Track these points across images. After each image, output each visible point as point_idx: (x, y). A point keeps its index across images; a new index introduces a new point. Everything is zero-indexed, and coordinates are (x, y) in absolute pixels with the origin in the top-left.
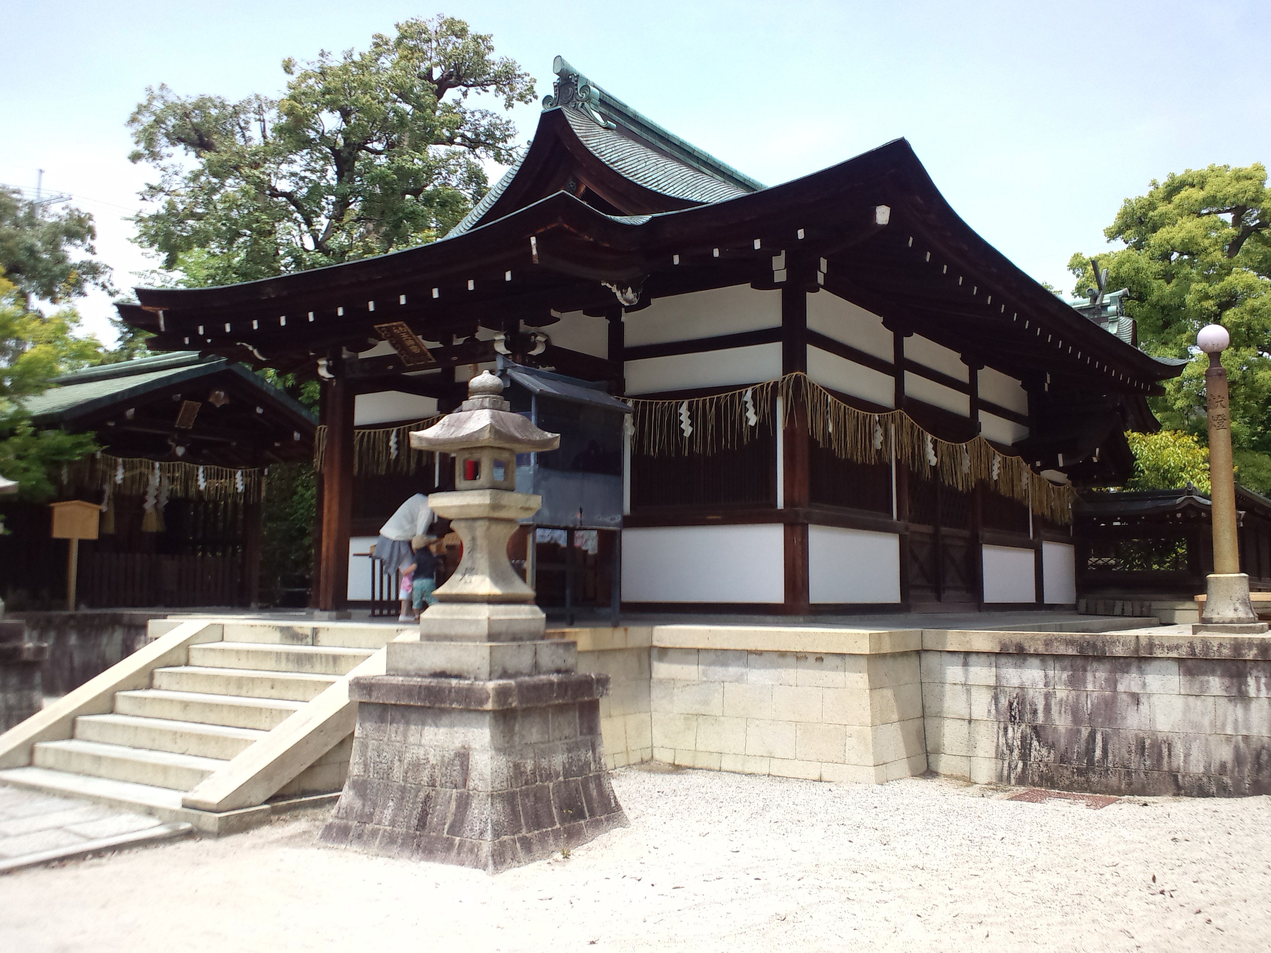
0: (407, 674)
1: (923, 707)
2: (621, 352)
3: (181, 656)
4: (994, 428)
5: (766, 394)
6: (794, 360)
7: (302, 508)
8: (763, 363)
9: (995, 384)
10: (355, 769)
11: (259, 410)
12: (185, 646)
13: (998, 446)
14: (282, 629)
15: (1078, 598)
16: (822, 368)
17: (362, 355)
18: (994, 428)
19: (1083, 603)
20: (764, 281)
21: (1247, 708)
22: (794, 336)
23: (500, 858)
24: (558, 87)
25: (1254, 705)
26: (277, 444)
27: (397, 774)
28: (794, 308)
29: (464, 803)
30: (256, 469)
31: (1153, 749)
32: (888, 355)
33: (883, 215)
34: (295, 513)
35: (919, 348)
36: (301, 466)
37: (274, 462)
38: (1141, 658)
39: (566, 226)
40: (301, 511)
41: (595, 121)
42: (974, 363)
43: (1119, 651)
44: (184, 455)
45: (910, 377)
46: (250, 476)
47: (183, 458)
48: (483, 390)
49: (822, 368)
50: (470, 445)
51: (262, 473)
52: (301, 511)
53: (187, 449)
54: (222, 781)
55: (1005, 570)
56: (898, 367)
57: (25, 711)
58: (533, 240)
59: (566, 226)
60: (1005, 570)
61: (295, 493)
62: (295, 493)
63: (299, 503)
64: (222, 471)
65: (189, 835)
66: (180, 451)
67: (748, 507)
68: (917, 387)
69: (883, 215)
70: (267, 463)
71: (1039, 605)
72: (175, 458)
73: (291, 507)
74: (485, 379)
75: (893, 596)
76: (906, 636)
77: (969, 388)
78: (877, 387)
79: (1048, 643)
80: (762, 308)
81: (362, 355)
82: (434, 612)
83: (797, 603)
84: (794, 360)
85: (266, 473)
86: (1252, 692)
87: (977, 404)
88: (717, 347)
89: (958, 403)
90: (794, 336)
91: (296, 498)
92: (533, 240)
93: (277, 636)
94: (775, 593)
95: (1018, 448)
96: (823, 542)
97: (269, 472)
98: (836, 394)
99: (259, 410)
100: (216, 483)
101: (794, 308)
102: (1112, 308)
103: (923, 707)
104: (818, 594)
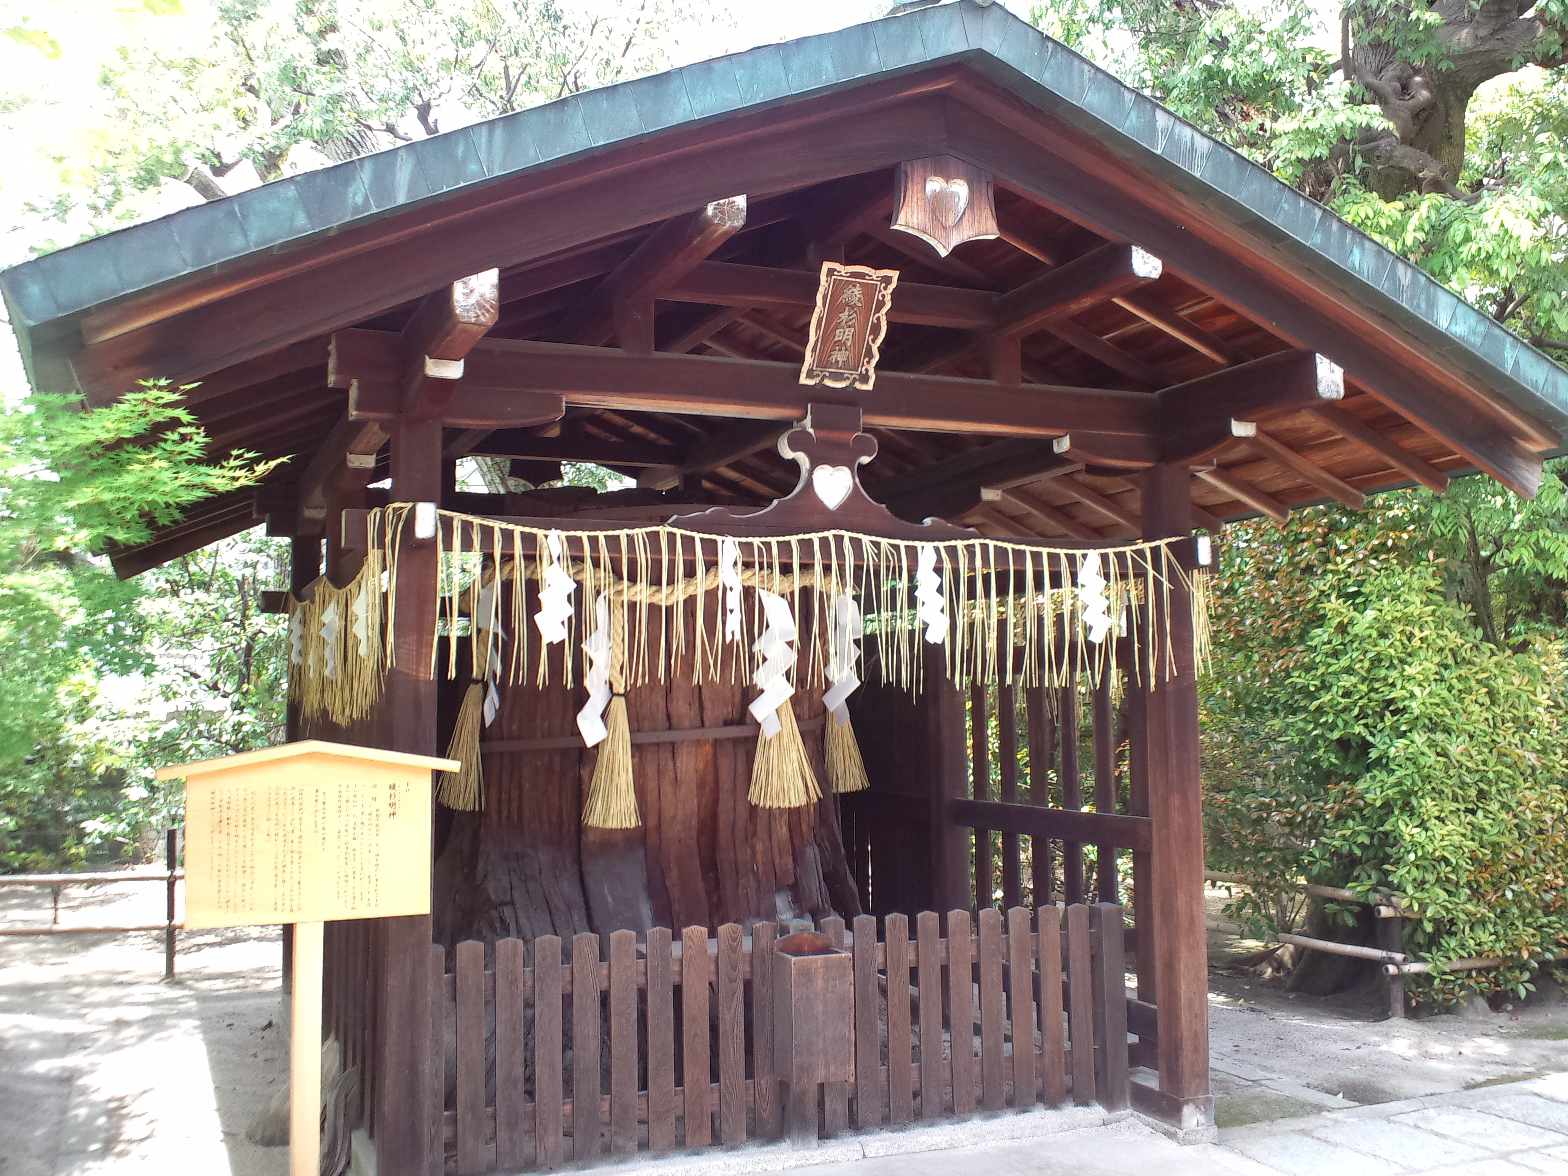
1: (660, 819)
7: (1349, 670)
11: (1146, 265)
26: (1241, 429)
30: (1162, 543)
34: (1325, 686)
36: (1334, 527)
37: (1236, 512)
39: (323, 568)
40: (1347, 681)
44: (848, 505)
46: (1140, 574)
47: (845, 517)
51: (1186, 554)
52: (1347, 681)
53: (863, 472)
57: (664, 1131)
59: (323, 568)
61: (1320, 620)
62: (1320, 620)
63: (1336, 654)
64: (1019, 556)
66: (833, 485)
70: (1213, 516)
73: (1309, 668)
85: (1204, 556)
91: (1320, 635)
97: (1215, 551)
99: (1146, 265)
100: (985, 611)
103: (660, 819)
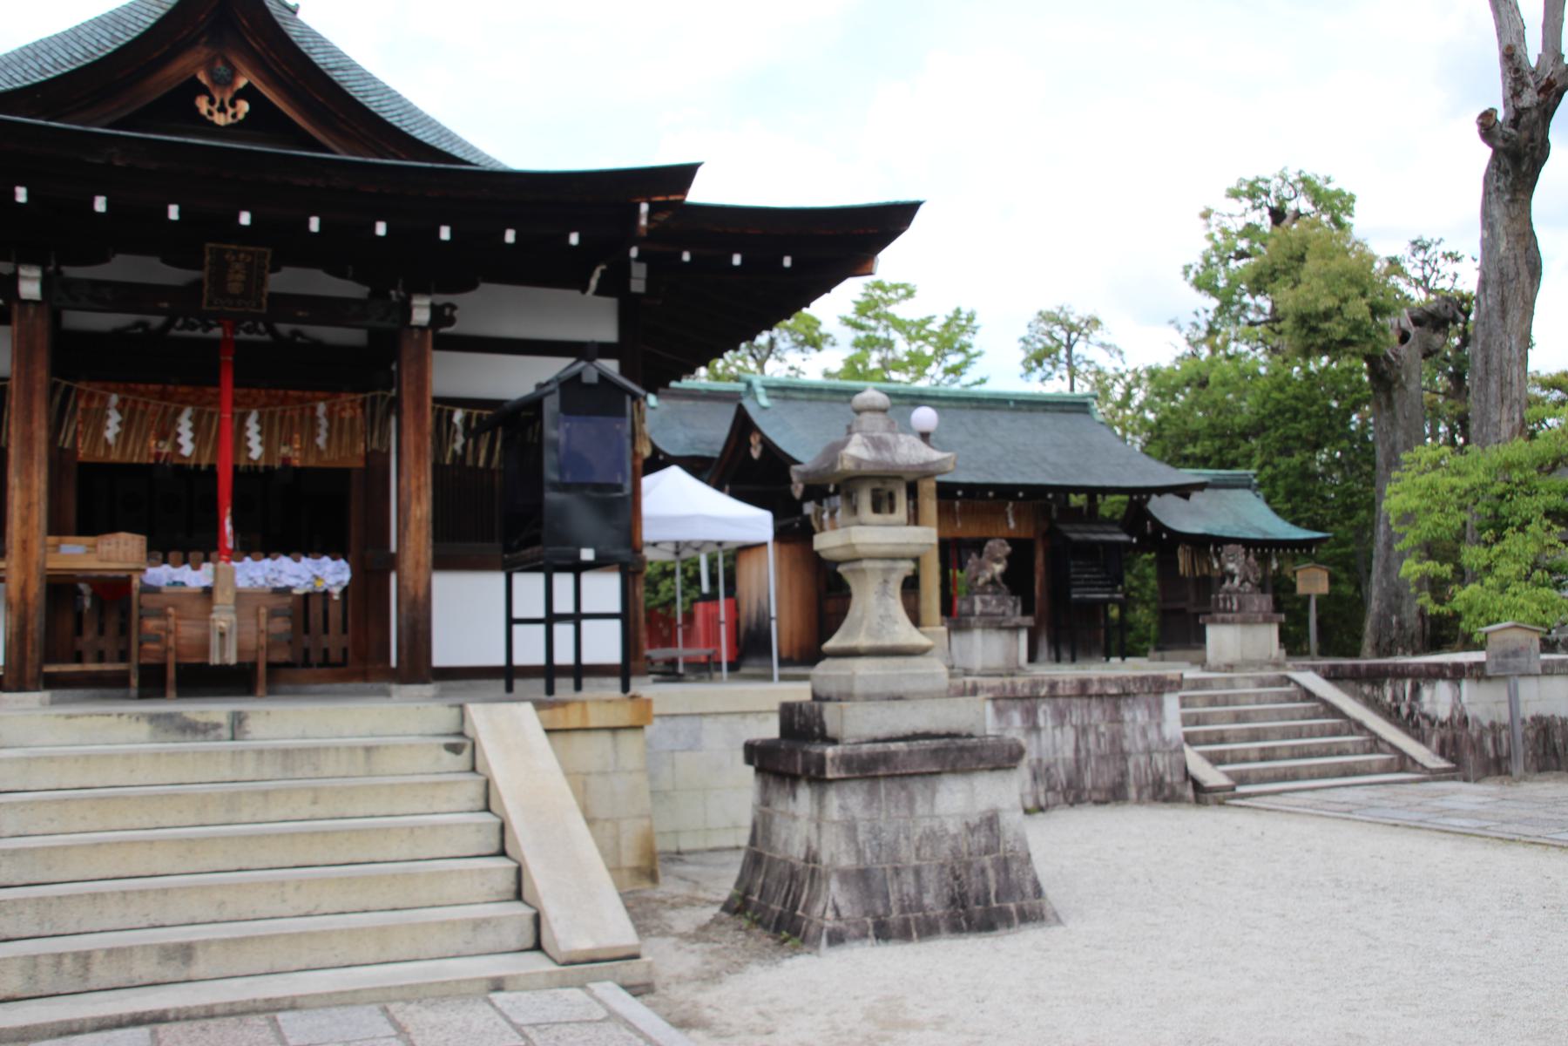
0: (875, 741)
21: (1039, 737)
25: (1043, 734)
27: (906, 854)
58: (644, 207)
86: (1041, 721)
92: (644, 207)
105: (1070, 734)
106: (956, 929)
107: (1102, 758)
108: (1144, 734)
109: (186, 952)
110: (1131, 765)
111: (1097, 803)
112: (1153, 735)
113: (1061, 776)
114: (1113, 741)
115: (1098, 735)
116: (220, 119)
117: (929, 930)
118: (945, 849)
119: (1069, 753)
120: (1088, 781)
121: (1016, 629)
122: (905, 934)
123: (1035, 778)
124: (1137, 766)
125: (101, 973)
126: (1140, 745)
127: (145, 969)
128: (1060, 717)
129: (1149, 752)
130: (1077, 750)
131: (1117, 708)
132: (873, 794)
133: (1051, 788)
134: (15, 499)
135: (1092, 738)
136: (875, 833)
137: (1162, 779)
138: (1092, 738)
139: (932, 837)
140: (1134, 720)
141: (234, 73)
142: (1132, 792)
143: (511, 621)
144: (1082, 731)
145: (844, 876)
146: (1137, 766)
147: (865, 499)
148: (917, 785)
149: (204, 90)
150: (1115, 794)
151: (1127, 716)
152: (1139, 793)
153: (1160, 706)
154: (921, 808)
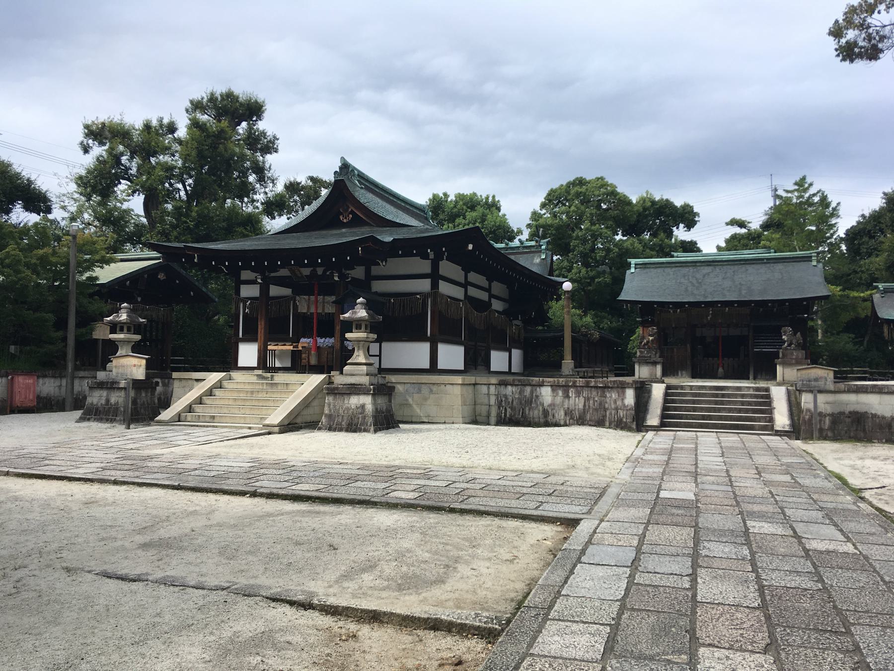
2: (370, 277)
3: (219, 385)
4: (497, 305)
5: (425, 296)
6: (435, 286)
8: (425, 285)
9: (498, 288)
10: (326, 411)
12: (220, 381)
13: (497, 311)
14: (257, 375)
15: (524, 370)
16: (445, 288)
17: (272, 274)
18: (497, 305)
19: (526, 373)
20: (425, 257)
22: (435, 277)
23: (375, 431)
24: (340, 168)
28: (435, 266)
29: (364, 418)
31: (623, 613)
32: (462, 281)
33: (470, 247)
35: (473, 277)
38: (541, 385)
41: (356, 184)
42: (490, 280)
43: (534, 383)
45: (462, 298)
47: (140, 302)
48: (361, 303)
49: (445, 288)
50: (361, 320)
54: (277, 417)
55: (498, 360)
56: (465, 285)
60: (498, 360)
65: (269, 433)
67: (417, 336)
68: (473, 292)
69: (470, 247)
71: (509, 373)
72: (137, 302)
74: (361, 300)
75: (461, 367)
76: (470, 379)
77: (488, 290)
78: (457, 292)
79: (514, 380)
80: (425, 266)
81: (272, 274)
82: (346, 368)
83: (433, 369)
84: (435, 286)
87: (491, 296)
88: (409, 280)
89: (484, 296)
90: (435, 277)
93: (255, 378)
94: (426, 365)
95: (504, 312)
96: (442, 348)
98: (449, 297)
101: (435, 266)
102: (543, 247)
104: (441, 366)
105: (582, 400)
106: (347, 431)
107: (596, 410)
108: (615, 402)
109: (213, 417)
110: (608, 413)
111: (590, 425)
112: (619, 403)
113: (577, 414)
114: (600, 404)
115: (594, 401)
116: (345, 221)
117: (341, 430)
118: (350, 412)
119: (581, 406)
120: (588, 417)
121: (655, 363)
122: (335, 430)
123: (566, 414)
124: (611, 414)
125: (201, 419)
126: (613, 406)
127: (207, 419)
128: (578, 394)
129: (617, 409)
130: (585, 405)
131: (604, 392)
132: (335, 397)
133: (572, 418)
134: (259, 327)
135: (591, 402)
136: (335, 406)
137: (621, 420)
138: (591, 402)
139: (348, 409)
140: (611, 397)
141: (348, 207)
142: (607, 424)
143: (380, 356)
144: (587, 399)
145: (326, 415)
146: (611, 414)
147: (125, 330)
148: (346, 396)
149: (342, 214)
150: (600, 423)
151: (608, 395)
152: (610, 423)
153: (624, 393)
154: (346, 402)
